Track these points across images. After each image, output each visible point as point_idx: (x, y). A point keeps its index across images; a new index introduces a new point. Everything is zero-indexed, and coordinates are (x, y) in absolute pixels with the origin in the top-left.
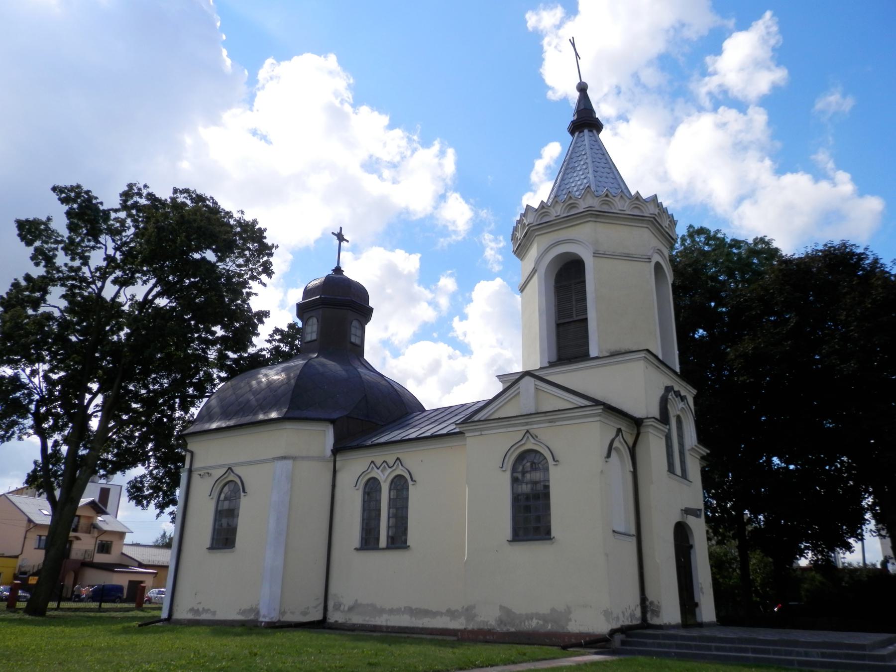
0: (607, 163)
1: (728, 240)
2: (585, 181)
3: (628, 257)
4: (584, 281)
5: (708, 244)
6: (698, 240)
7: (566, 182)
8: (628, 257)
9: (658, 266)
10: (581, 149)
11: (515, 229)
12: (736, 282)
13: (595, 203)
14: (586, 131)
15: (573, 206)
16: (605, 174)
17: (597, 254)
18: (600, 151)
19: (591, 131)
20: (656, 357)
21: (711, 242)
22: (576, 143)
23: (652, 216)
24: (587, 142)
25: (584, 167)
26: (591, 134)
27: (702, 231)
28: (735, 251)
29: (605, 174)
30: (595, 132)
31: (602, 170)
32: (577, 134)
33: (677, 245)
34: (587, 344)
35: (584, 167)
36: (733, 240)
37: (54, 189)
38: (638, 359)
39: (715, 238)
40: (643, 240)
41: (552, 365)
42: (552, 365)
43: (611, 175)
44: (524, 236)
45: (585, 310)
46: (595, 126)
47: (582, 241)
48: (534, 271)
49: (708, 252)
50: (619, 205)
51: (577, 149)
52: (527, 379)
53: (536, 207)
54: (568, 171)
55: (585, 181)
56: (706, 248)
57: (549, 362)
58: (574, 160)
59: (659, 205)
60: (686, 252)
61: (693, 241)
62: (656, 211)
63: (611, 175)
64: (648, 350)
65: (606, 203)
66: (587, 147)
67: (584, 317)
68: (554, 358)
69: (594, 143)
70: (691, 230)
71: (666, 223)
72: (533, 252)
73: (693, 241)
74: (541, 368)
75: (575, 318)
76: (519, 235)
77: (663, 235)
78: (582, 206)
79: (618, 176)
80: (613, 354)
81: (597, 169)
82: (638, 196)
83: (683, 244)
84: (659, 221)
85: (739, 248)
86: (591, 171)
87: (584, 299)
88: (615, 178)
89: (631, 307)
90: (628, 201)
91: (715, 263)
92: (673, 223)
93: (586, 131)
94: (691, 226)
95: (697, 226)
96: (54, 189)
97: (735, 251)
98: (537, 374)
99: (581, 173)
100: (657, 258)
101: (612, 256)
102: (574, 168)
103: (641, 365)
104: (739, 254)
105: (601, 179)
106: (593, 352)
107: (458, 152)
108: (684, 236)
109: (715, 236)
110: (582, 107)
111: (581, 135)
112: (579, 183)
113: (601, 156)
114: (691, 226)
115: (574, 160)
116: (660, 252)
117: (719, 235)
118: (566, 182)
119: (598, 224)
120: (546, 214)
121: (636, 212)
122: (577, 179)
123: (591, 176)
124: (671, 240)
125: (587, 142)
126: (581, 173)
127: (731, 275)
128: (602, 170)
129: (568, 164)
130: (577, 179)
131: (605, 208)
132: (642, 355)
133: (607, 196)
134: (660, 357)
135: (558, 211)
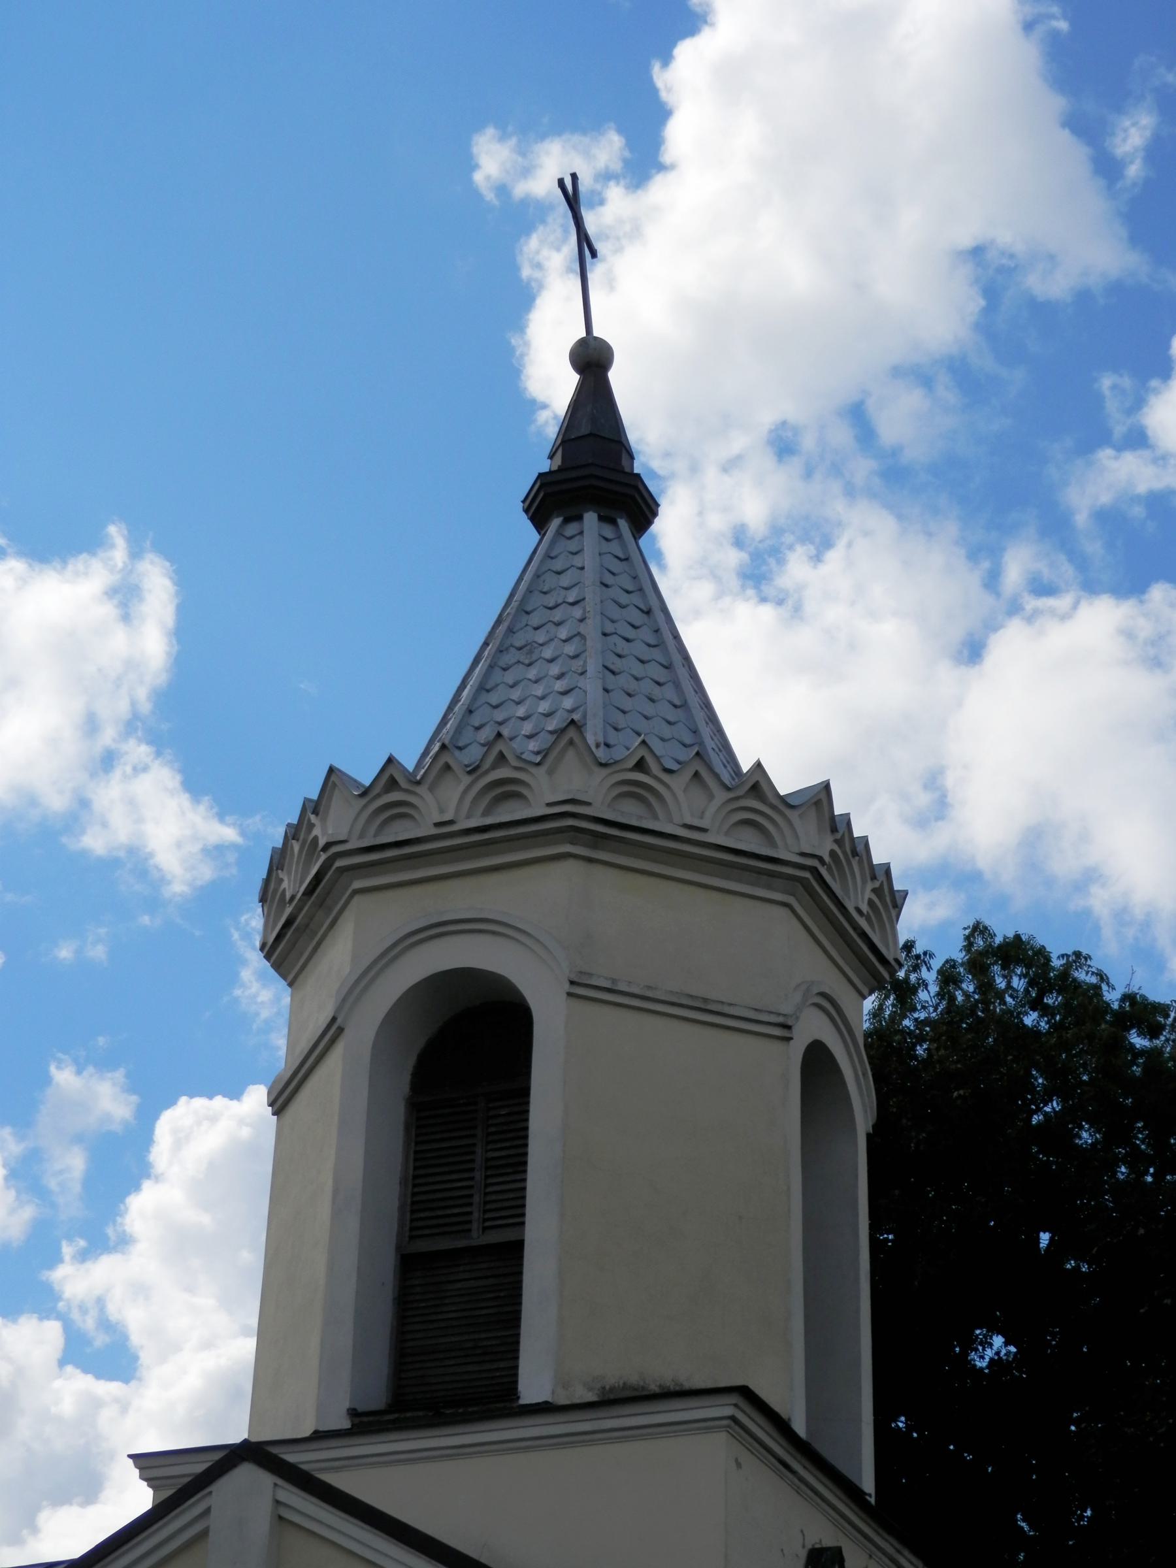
0: (659, 645)
1: (1112, 997)
2: (568, 702)
3: (704, 1012)
4: (525, 1092)
5: (1037, 1004)
6: (1001, 983)
7: (494, 698)
8: (704, 1012)
9: (817, 1061)
10: (565, 580)
11: (278, 861)
12: (1137, 1161)
13: (595, 791)
14: (590, 518)
15: (506, 791)
16: (647, 687)
17: (581, 989)
18: (635, 599)
19: (613, 522)
20: (781, 1425)
21: (1049, 1000)
22: (549, 556)
23: (809, 865)
24: (588, 559)
25: (570, 649)
26: (608, 531)
27: (1016, 952)
28: (1138, 1041)
29: (647, 687)
30: (623, 524)
31: (638, 669)
32: (556, 523)
33: (923, 995)
34: (508, 1349)
35: (570, 649)
36: (1129, 997)
37: (130, 1456)
38: (705, 1425)
39: (1065, 982)
40: (769, 953)
41: (363, 1423)
42: (363, 1423)
43: (669, 692)
44: (309, 892)
45: (513, 1209)
46: (635, 506)
47: (534, 931)
48: (332, 1032)
49: (1034, 1032)
50: (684, 808)
51: (550, 581)
52: (247, 1474)
53: (366, 780)
54: (507, 659)
55: (568, 702)
56: (1030, 1019)
57: (353, 1413)
58: (535, 620)
59: (839, 827)
60: (951, 1024)
61: (986, 986)
62: (825, 847)
63: (669, 692)
64: (746, 1393)
65: (635, 792)
66: (590, 577)
67: (508, 1235)
68: (377, 1398)
69: (616, 566)
70: (980, 942)
71: (858, 898)
72: (339, 956)
73: (986, 986)
74: (319, 1436)
75: (479, 1238)
76: (292, 884)
77: (850, 943)
78: (543, 793)
79: (694, 701)
80: (613, 1399)
81: (617, 664)
82: (757, 783)
83: (944, 993)
84: (836, 887)
85: (1153, 1031)
86: (593, 665)
87: (520, 1164)
88: (683, 706)
89: (694, 1206)
90: (721, 796)
91: (1061, 1084)
92: (889, 900)
93: (590, 518)
94: (978, 929)
95: (1002, 931)
96: (130, 1456)
97: (1138, 1041)
98: (292, 1457)
99: (555, 670)
100: (813, 1027)
101: (643, 1003)
102: (528, 647)
103: (716, 1450)
104: (1153, 1055)
105: (627, 704)
106: (534, 1384)
107: (184, 581)
108: (951, 964)
109: (1065, 974)
110: (584, 430)
111: (572, 529)
112: (544, 707)
113: (637, 617)
114: (978, 929)
115: (535, 620)
116: (829, 1006)
117: (1081, 975)
118: (494, 698)
119: (599, 871)
120: (400, 811)
121: (748, 841)
122: (539, 690)
123: (592, 686)
124: (874, 959)
125: (588, 559)
126: (555, 670)
127: (1117, 1134)
128: (638, 669)
129: (511, 631)
130: (539, 690)
131: (630, 813)
132: (723, 1408)
133: (640, 766)
134: (800, 1427)
135: (448, 804)
